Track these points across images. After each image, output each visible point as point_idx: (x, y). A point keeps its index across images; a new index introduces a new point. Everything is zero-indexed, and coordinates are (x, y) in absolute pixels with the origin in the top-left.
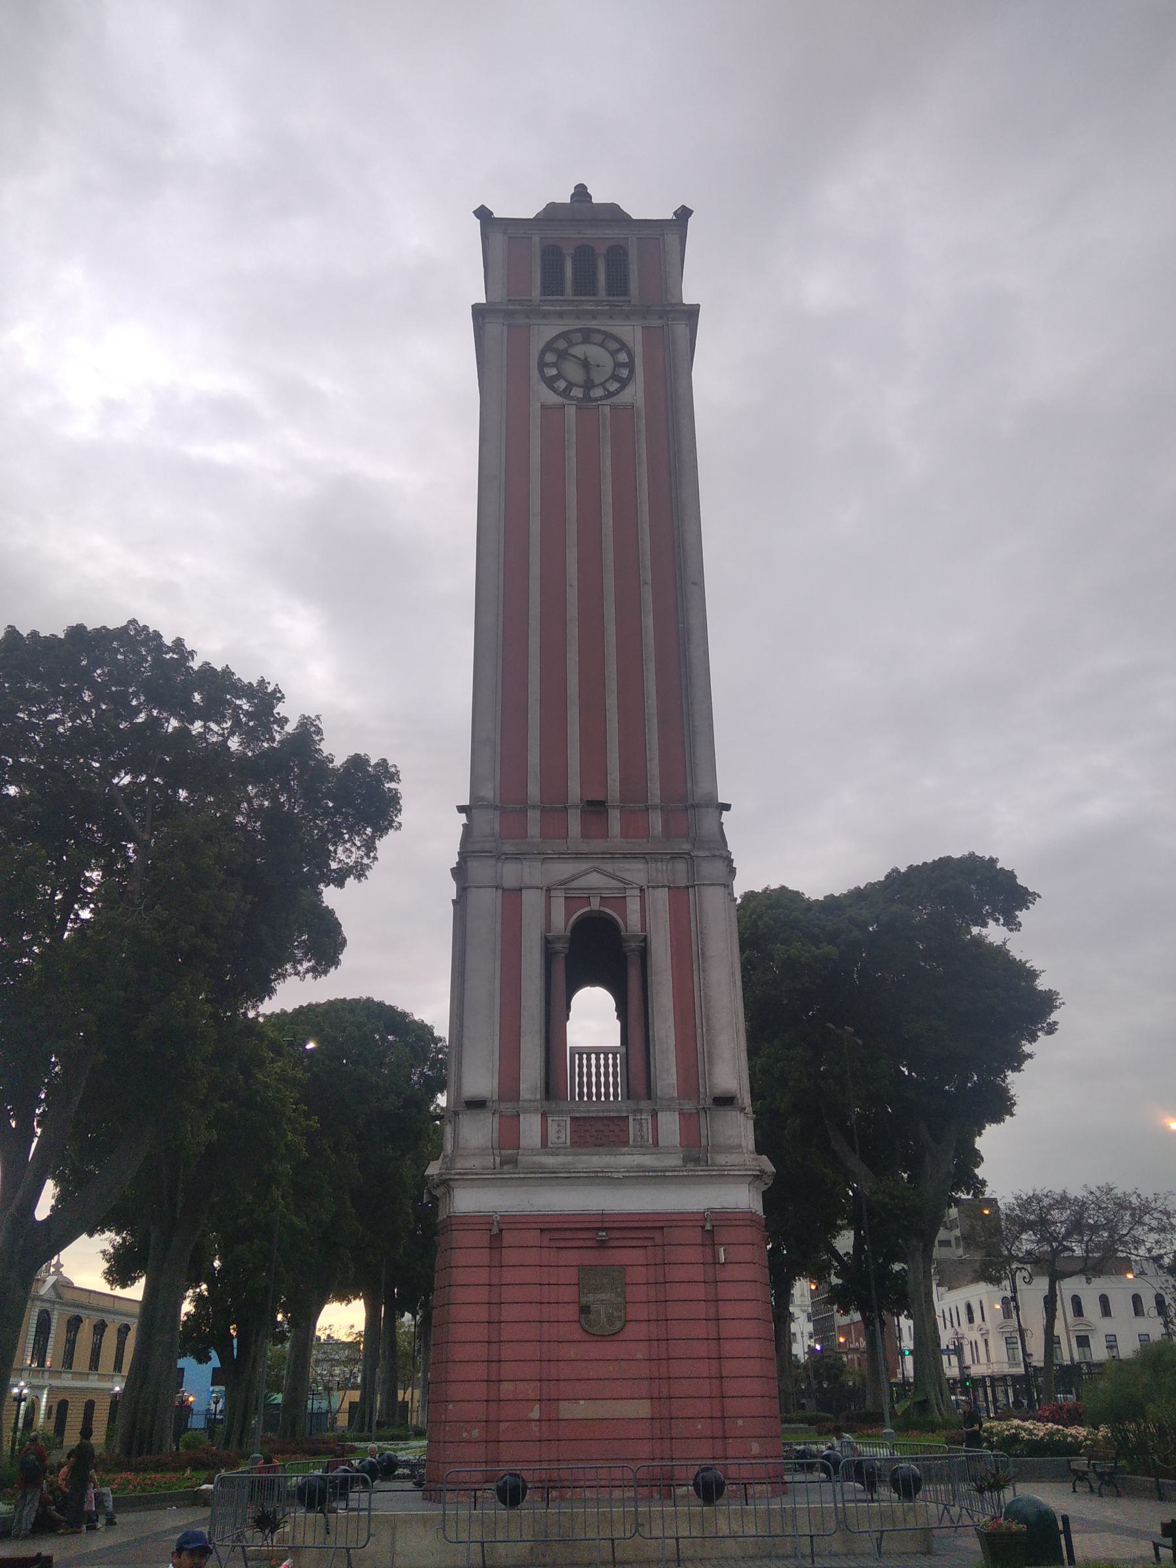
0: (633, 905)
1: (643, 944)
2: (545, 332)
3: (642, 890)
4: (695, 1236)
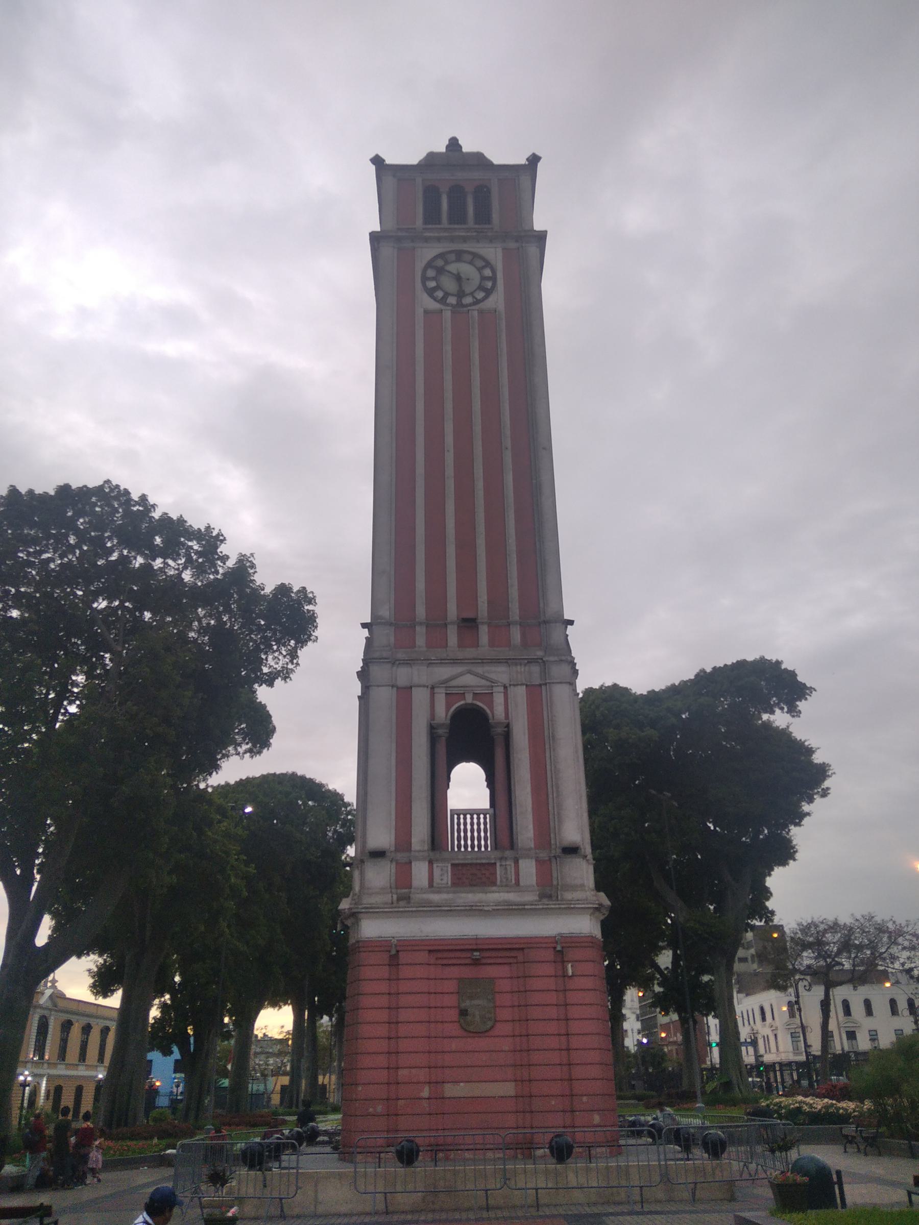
0: (499, 699)
1: (506, 729)
2: (427, 253)
3: (505, 687)
4: (549, 955)
